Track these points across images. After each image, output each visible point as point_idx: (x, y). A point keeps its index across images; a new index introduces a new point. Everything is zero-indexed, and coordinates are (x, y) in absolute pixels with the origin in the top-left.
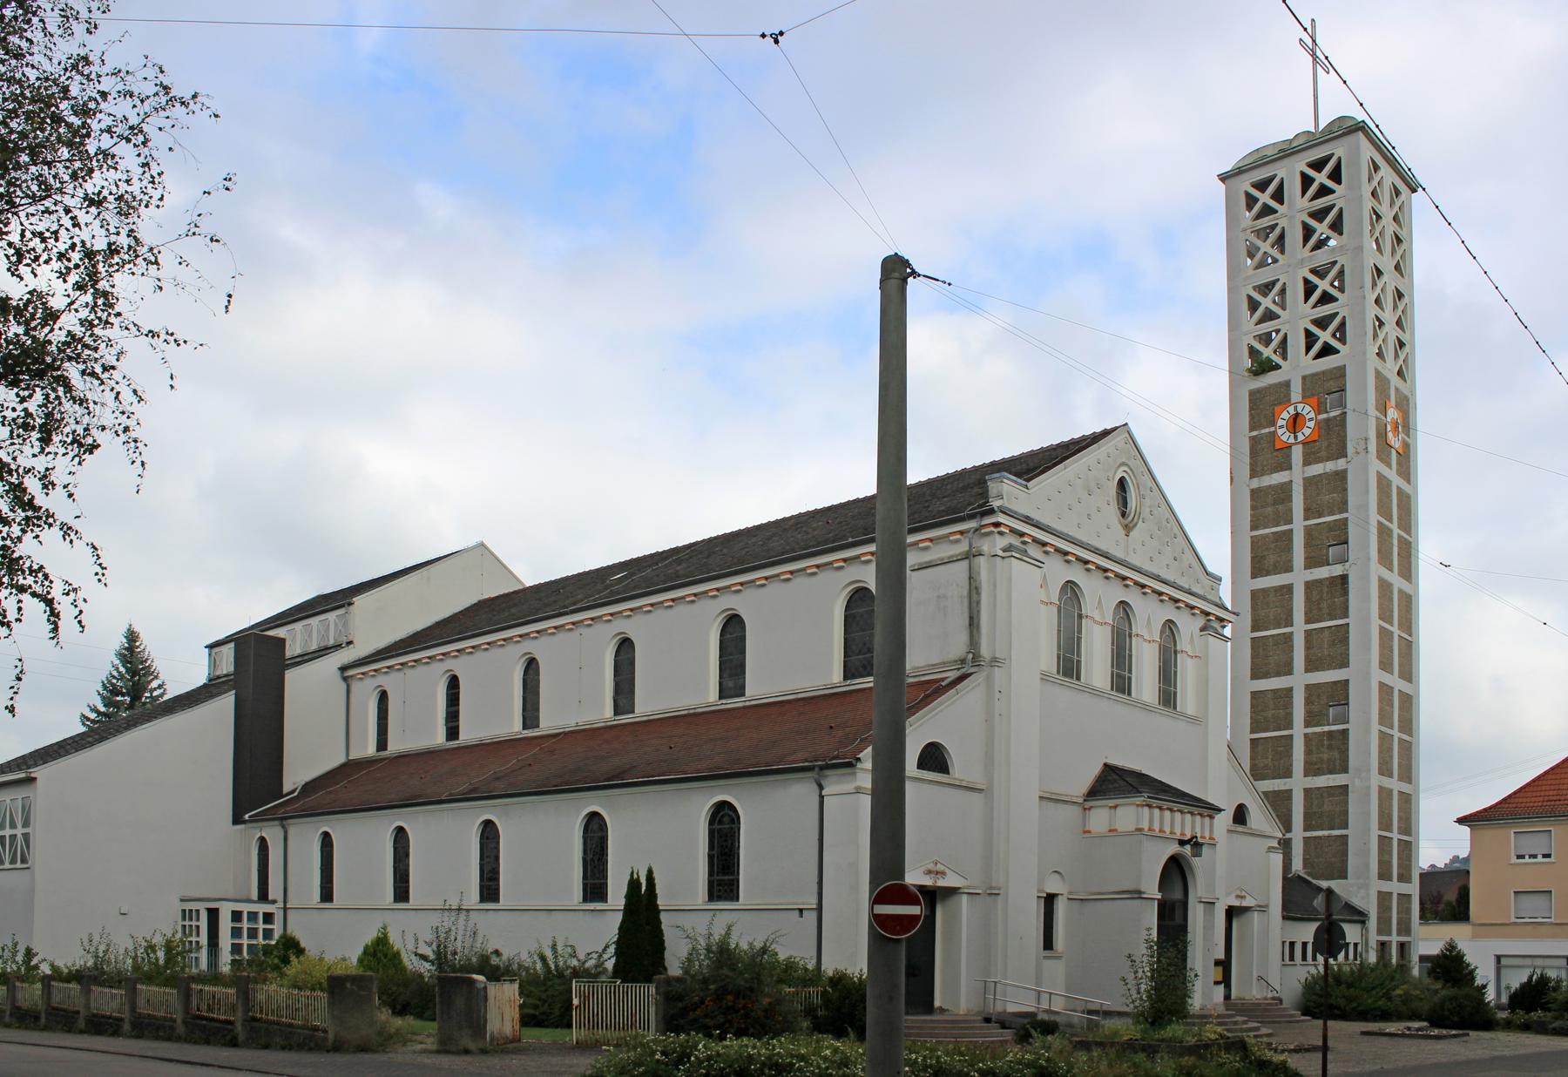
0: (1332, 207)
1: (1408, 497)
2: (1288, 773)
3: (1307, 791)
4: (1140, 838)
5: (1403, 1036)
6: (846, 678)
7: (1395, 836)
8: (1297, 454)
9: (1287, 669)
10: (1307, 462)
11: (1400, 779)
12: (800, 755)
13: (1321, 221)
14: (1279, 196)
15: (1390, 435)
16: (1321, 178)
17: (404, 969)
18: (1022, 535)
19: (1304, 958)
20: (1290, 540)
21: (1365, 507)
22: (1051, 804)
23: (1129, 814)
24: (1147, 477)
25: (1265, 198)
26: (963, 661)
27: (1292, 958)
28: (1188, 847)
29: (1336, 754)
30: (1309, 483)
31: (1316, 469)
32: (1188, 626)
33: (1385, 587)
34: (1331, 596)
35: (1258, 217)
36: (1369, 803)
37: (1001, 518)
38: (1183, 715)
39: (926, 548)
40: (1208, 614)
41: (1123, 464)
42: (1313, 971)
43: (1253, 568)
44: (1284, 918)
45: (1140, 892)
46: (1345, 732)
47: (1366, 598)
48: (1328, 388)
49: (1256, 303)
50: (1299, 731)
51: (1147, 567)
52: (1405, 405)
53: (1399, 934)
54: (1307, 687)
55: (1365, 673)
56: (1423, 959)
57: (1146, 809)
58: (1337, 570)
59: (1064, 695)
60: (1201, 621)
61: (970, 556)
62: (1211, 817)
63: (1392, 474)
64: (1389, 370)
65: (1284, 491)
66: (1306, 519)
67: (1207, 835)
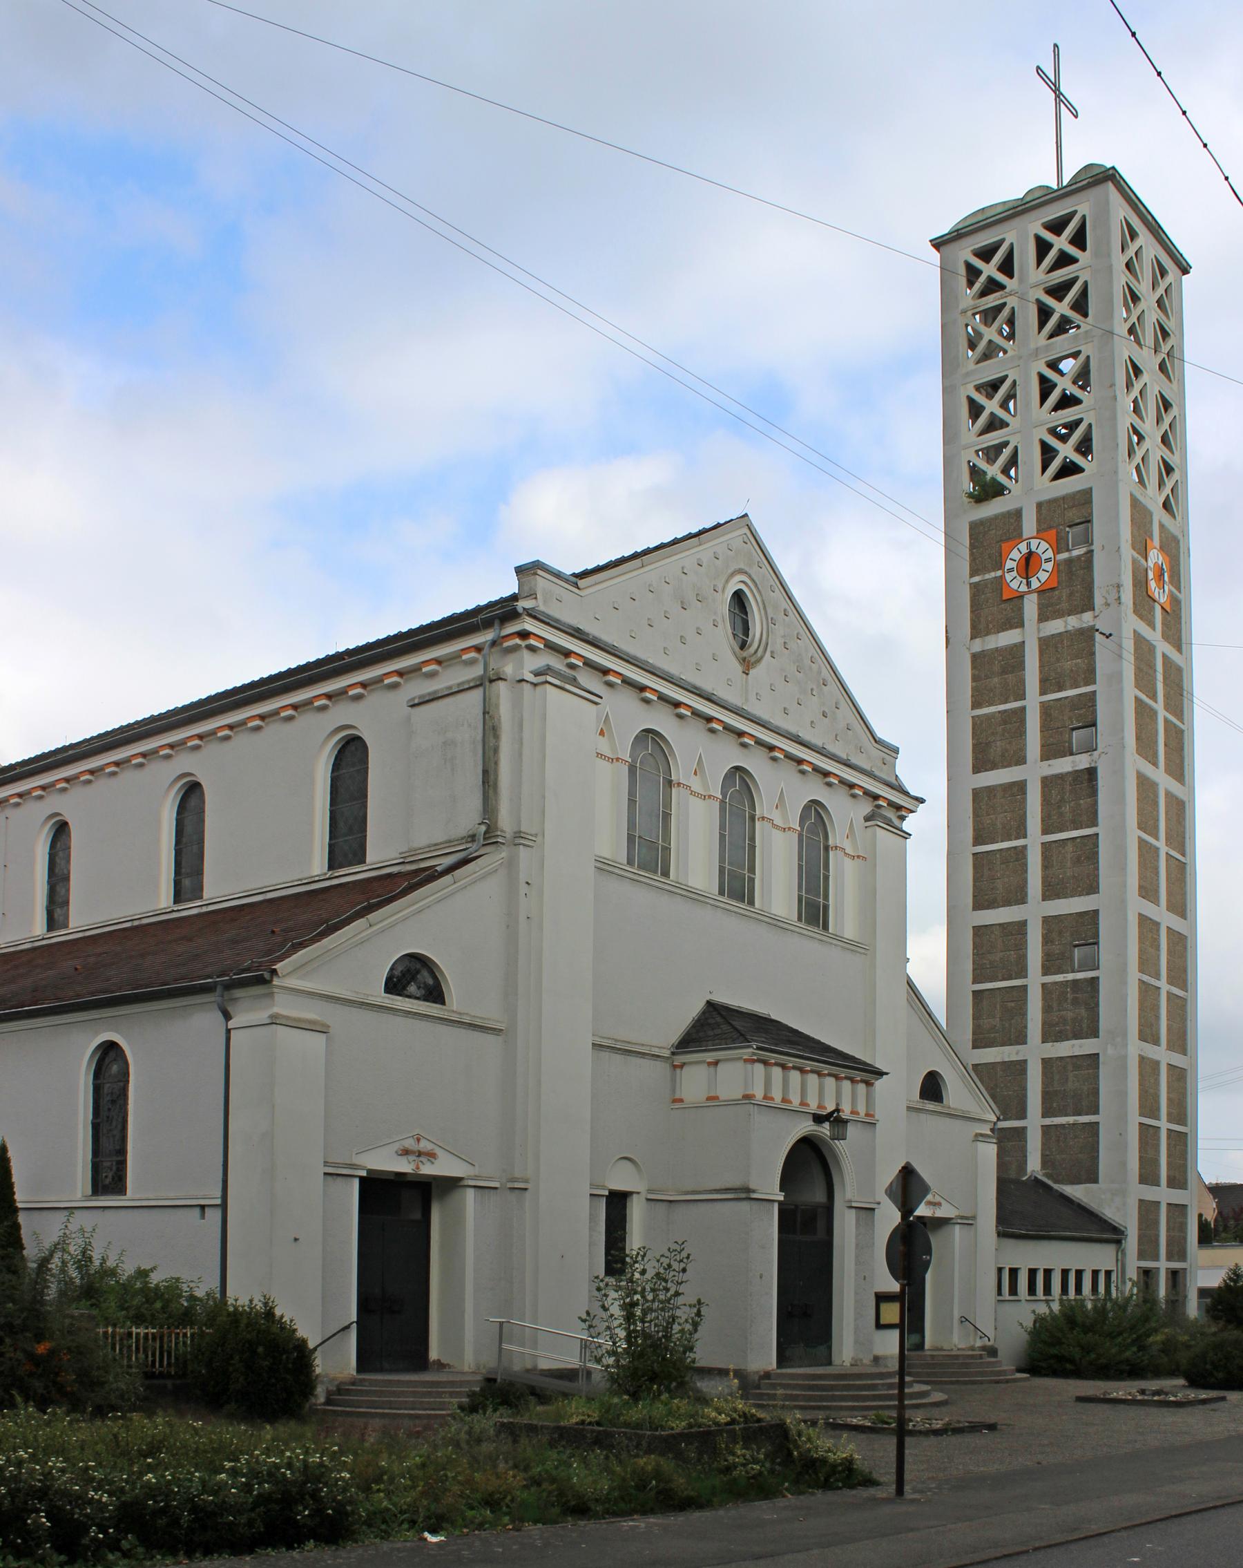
0: (1073, 281)
1: (1179, 670)
2: (1021, 1039)
3: (1046, 1062)
4: (764, 1111)
5: (1134, 1402)
6: (331, 867)
7: (1164, 1124)
8: (1031, 607)
9: (1018, 896)
10: (1043, 617)
11: (1170, 1047)
12: (209, 970)
13: (1060, 299)
14: (1007, 267)
15: (1153, 584)
16: (1061, 243)
17: (1220, 1287)
18: (567, 653)
19: (1032, 1290)
20: (1023, 721)
21: (1117, 677)
22: (618, 1058)
23: (736, 1074)
24: (778, 594)
25: (989, 270)
26: (473, 838)
27: (1013, 1290)
28: (827, 1125)
29: (1083, 1012)
30: (1046, 644)
31: (1056, 626)
32: (845, 814)
33: (1146, 787)
34: (1076, 796)
35: (983, 293)
36: (1125, 1077)
37: (529, 625)
38: (838, 938)
39: (432, 675)
40: (876, 797)
41: (741, 571)
42: (1042, 1309)
43: (975, 759)
44: (1001, 1235)
45: (748, 1190)
46: (1094, 982)
47: (1120, 799)
48: (1070, 518)
49: (978, 406)
50: (1035, 979)
51: (778, 721)
52: (1174, 548)
53: (1169, 1258)
54: (1046, 920)
55: (1120, 901)
56: (1203, 1292)
57: (759, 1067)
58: (1082, 762)
59: (639, 898)
60: (866, 807)
61: (489, 680)
62: (868, 1084)
63: (1155, 636)
64: (1153, 498)
65: (1015, 655)
66: (1043, 693)
67: (862, 1110)
